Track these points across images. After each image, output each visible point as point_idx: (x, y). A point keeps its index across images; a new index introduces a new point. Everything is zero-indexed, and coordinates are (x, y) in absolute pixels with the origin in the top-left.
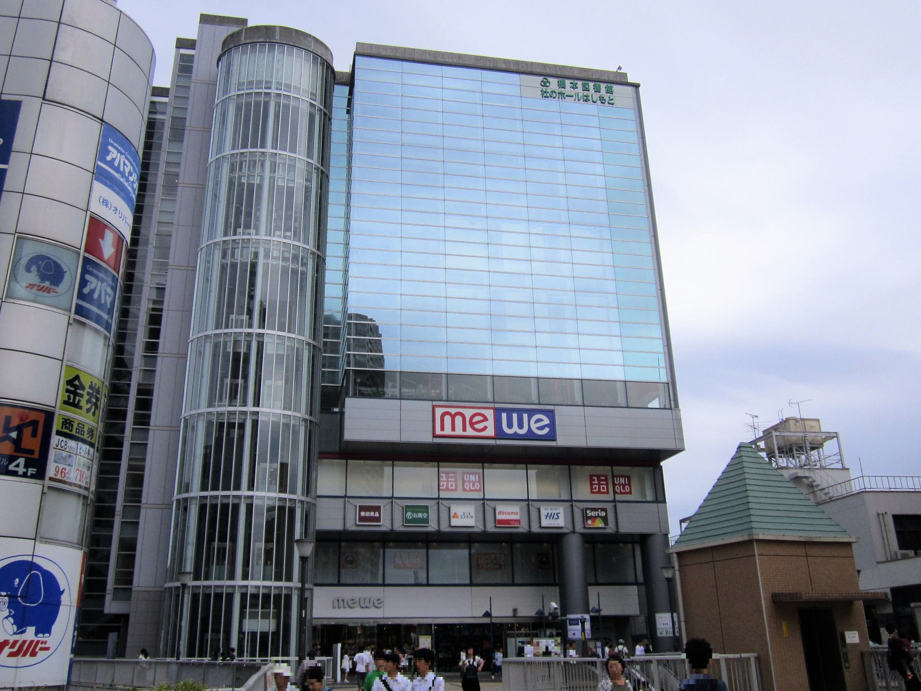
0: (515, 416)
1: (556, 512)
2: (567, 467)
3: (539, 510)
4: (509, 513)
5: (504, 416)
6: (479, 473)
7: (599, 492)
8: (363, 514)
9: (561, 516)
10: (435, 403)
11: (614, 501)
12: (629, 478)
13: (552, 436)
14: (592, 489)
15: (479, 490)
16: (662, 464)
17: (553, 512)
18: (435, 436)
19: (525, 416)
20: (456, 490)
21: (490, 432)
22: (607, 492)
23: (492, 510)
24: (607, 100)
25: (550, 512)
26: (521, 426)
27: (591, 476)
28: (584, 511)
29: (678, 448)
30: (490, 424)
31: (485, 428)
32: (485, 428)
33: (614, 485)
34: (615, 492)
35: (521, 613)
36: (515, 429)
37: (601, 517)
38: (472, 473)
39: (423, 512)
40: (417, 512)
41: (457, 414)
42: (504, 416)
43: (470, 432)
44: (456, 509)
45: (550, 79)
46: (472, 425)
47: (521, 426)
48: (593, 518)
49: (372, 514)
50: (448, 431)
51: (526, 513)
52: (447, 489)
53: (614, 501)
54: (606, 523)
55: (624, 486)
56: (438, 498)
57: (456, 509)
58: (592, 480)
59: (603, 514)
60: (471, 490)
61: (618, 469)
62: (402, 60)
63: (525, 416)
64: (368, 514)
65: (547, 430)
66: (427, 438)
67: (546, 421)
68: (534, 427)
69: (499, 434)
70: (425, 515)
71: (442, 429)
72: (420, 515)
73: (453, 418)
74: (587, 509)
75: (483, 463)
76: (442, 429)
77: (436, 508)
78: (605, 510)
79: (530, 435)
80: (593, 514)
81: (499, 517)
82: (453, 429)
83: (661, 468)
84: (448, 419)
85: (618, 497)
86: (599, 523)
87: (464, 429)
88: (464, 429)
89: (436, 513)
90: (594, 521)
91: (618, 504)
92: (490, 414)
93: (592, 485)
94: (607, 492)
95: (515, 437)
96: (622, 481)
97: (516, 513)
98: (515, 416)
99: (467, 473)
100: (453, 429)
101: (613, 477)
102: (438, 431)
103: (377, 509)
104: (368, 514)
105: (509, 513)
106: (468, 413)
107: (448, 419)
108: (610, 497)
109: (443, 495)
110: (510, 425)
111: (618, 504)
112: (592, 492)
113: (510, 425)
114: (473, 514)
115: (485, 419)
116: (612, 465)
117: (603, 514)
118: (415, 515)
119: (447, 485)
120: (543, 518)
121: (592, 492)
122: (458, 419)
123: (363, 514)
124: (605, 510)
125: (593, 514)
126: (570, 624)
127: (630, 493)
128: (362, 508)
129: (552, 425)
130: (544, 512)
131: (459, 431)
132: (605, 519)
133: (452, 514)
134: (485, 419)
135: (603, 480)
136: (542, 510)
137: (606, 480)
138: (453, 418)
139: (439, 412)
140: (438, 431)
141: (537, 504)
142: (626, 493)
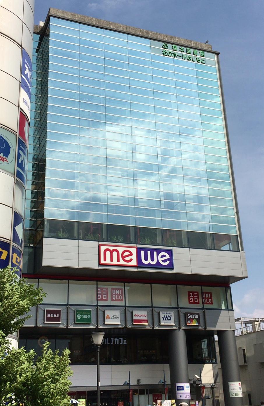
0: (149, 253)
1: (170, 315)
2: (175, 286)
3: (159, 314)
4: (141, 316)
5: (142, 252)
6: (122, 289)
7: (194, 303)
8: (49, 316)
9: (172, 318)
10: (100, 243)
11: (203, 308)
12: (211, 294)
13: (171, 266)
14: (189, 300)
15: (122, 300)
16: (230, 285)
17: (168, 315)
18: (100, 264)
19: (155, 253)
20: (107, 300)
21: (134, 263)
22: (198, 303)
23: (130, 313)
24: (201, 60)
25: (166, 315)
26: (152, 259)
27: (189, 292)
28: (185, 315)
29: (244, 276)
30: (134, 257)
31: (131, 260)
32: (131, 260)
33: (203, 298)
34: (203, 303)
35: (143, 383)
36: (149, 261)
37: (196, 319)
38: (118, 289)
39: (87, 315)
40: (84, 315)
41: (114, 250)
42: (142, 252)
43: (122, 262)
44: (108, 313)
45: (168, 45)
46: (123, 257)
47: (152, 259)
48: (192, 320)
49: (55, 316)
50: (108, 261)
51: (151, 316)
52: (102, 299)
53: (203, 308)
54: (199, 323)
55: (208, 299)
56: (97, 305)
57: (108, 313)
58: (189, 295)
59: (197, 317)
60: (116, 300)
61: (206, 289)
62: (79, 23)
63: (155, 253)
64: (52, 316)
65: (168, 262)
66: (94, 265)
67: (168, 257)
68: (160, 260)
69: (140, 264)
70: (89, 317)
71: (105, 260)
72: (86, 317)
73: (111, 252)
74: (188, 313)
75: (68, 279)
76: (105, 260)
77: (65, 311)
78: (198, 314)
79: (158, 265)
80: (191, 316)
81: (135, 318)
82: (112, 260)
83: (230, 288)
84: (108, 253)
85: (206, 306)
86: (195, 323)
87: (118, 261)
88: (118, 261)
89: (66, 314)
90: (192, 321)
91: (206, 311)
92: (134, 251)
93: (189, 298)
94: (198, 303)
95: (149, 266)
96: (207, 296)
97: (145, 316)
98: (149, 253)
99: (114, 289)
100: (112, 260)
101: (202, 293)
102: (102, 262)
103: (58, 312)
104: (52, 316)
105: (141, 316)
106: (121, 250)
107: (108, 253)
108: (200, 306)
109: (100, 303)
110: (146, 259)
111: (206, 311)
112: (190, 303)
113: (146, 259)
114: (119, 316)
115: (131, 254)
116: (151, 283)
117: (197, 317)
118: (82, 317)
119: (102, 296)
120: (161, 319)
121: (190, 303)
122: (115, 254)
123: (49, 316)
124: (198, 314)
125: (191, 316)
126: (178, 390)
127: (212, 303)
128: (49, 312)
129: (171, 259)
130: (162, 315)
131: (115, 262)
132: (198, 321)
133: (106, 316)
134: (131, 254)
135: (196, 295)
136: (161, 313)
137: (198, 295)
138: (111, 252)
139: (103, 248)
140: (102, 262)
141: (130, 309)
142: (209, 304)
